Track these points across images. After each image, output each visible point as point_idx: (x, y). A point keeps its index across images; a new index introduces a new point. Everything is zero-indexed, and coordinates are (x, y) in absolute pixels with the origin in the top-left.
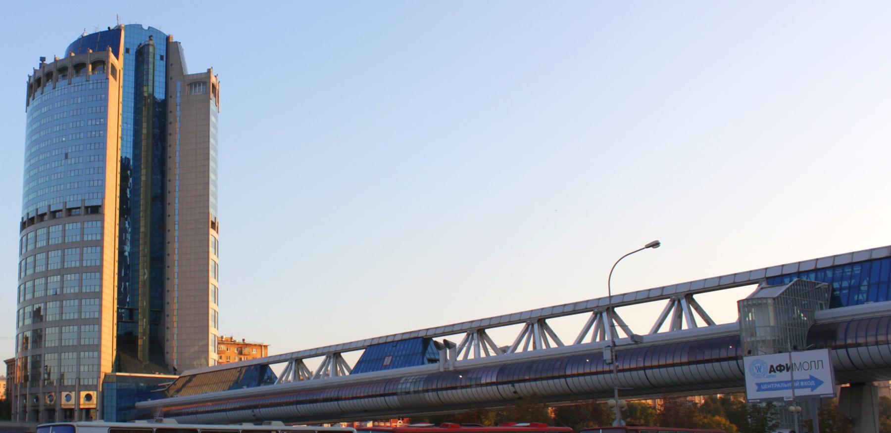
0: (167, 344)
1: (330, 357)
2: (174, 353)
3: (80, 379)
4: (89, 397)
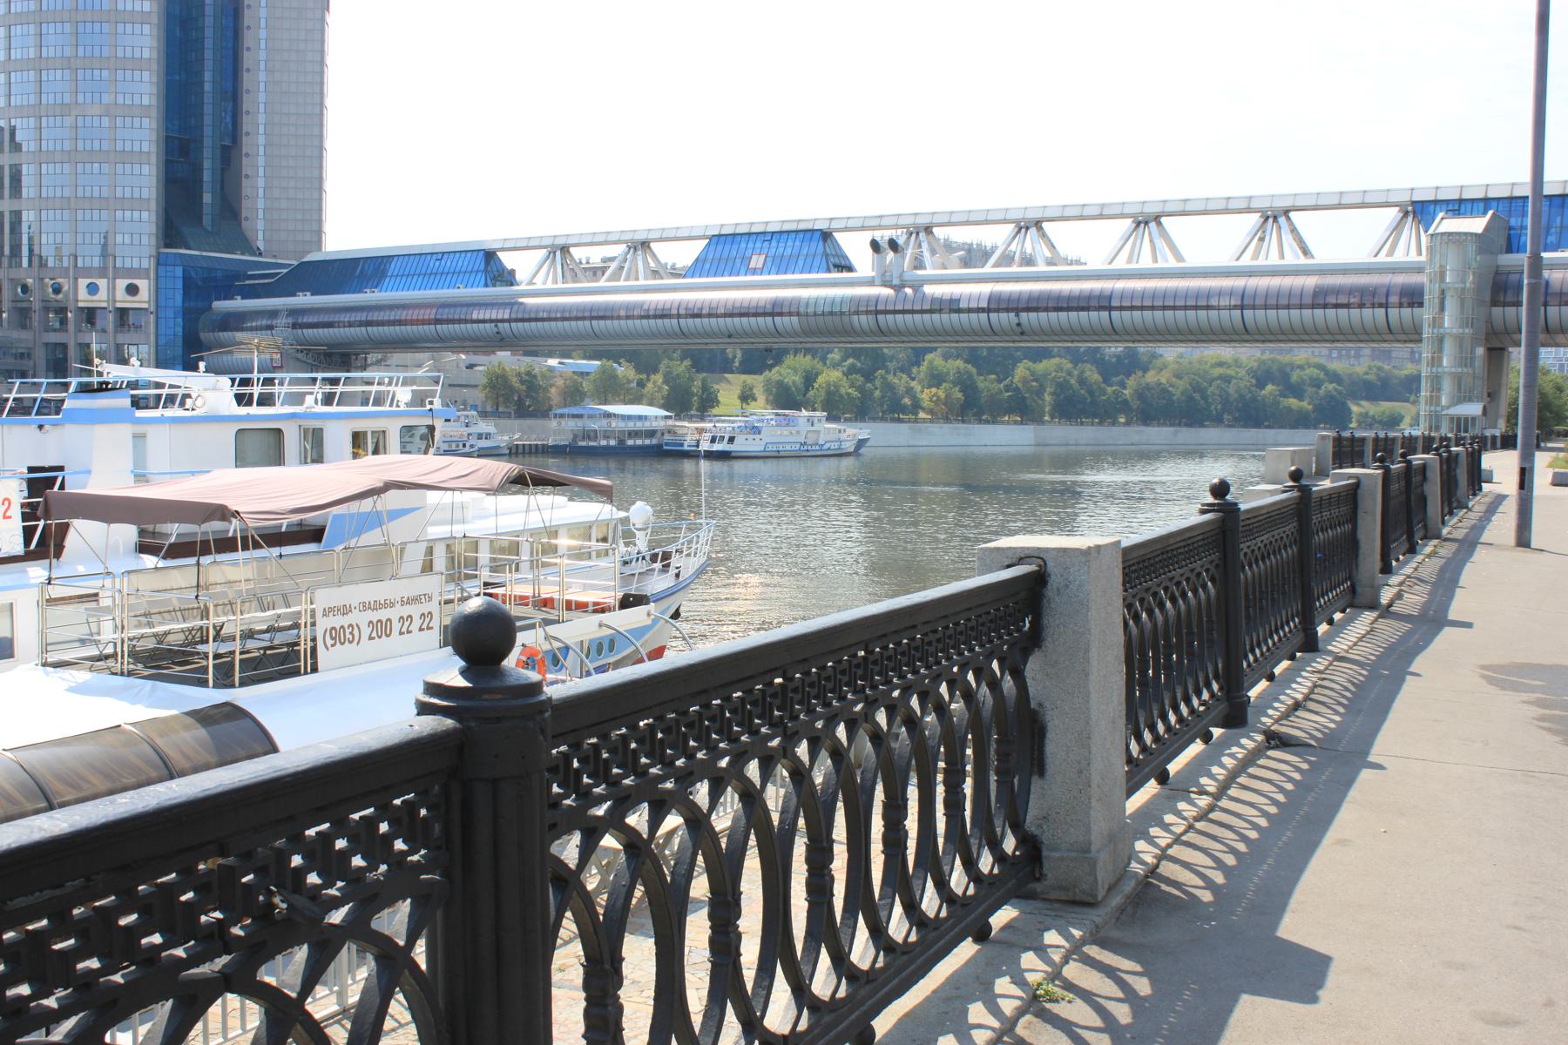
0: (245, 204)
1: (635, 250)
2: (230, 210)
3: (76, 257)
4: (132, 290)
